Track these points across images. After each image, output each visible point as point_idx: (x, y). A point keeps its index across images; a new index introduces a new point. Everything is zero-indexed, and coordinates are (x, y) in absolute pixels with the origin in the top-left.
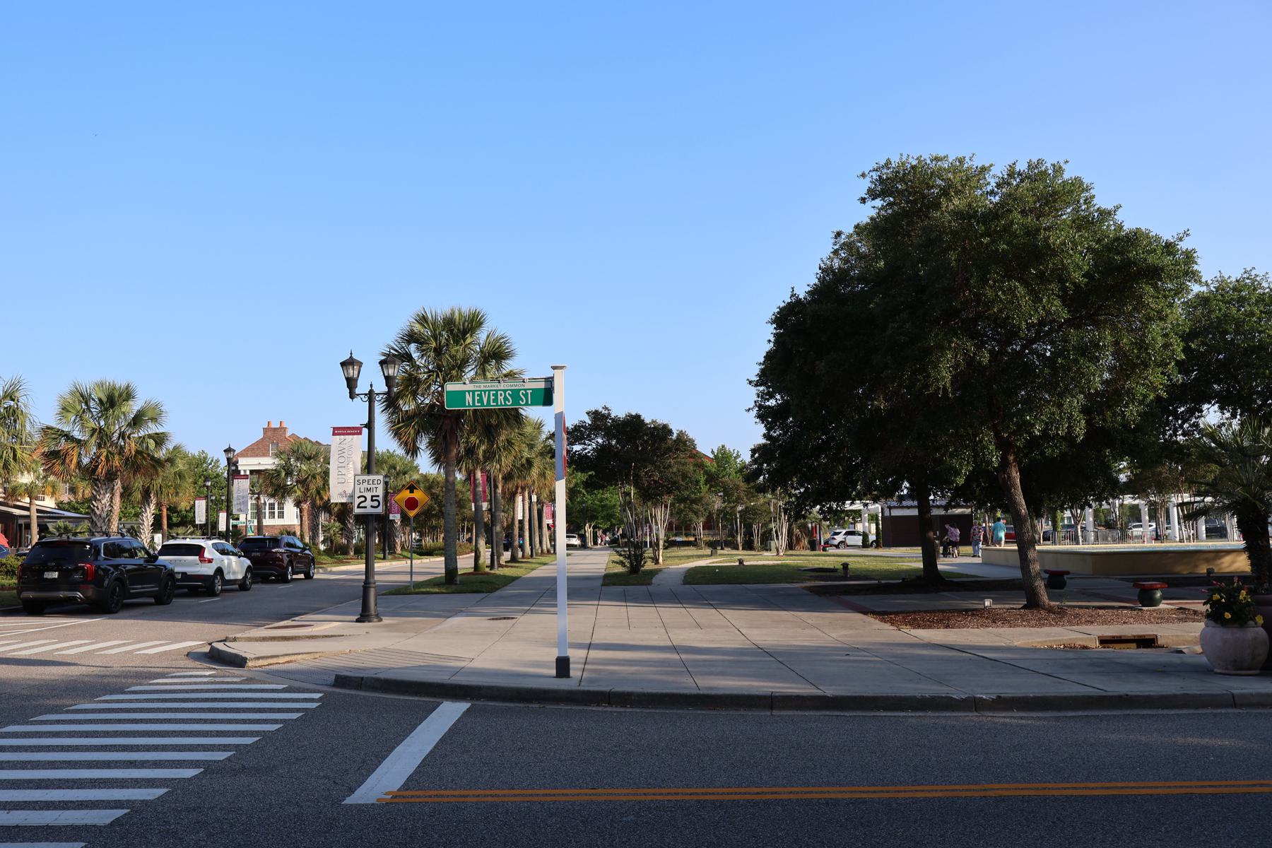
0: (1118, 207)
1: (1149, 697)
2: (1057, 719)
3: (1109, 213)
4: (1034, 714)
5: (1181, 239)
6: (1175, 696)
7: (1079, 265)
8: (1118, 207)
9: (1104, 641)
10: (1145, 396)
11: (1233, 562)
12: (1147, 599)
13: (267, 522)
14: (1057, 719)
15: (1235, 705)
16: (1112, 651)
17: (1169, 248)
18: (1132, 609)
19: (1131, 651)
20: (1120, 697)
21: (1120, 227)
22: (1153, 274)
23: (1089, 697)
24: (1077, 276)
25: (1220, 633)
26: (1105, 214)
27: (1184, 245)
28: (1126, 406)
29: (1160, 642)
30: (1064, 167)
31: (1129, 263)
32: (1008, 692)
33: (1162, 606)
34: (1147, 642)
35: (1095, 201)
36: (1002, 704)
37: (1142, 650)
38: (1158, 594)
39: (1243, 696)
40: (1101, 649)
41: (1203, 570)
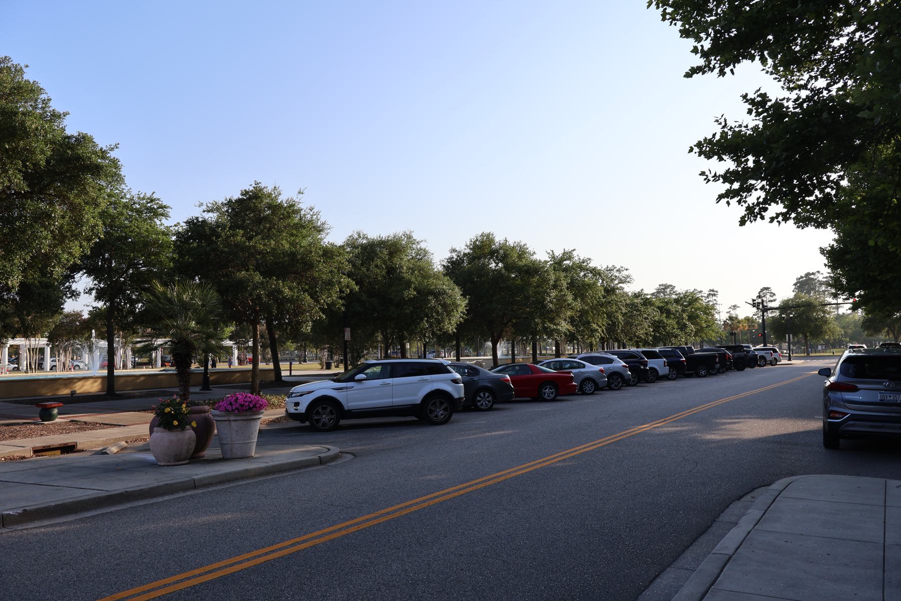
0: (65, 114)
1: (141, 490)
2: (82, 520)
3: (59, 117)
4: (46, 523)
5: (112, 149)
6: (158, 487)
7: (42, 154)
8: (65, 114)
9: (37, 451)
10: (68, 261)
11: (83, 386)
12: (46, 415)
13: (117, 372)
14: (82, 520)
15: (195, 487)
16: (47, 457)
17: (103, 154)
18: (35, 424)
19: (58, 455)
20: (122, 494)
21: (63, 130)
22: (96, 170)
23: (99, 498)
24: (41, 160)
25: (161, 435)
26: (56, 116)
27: (112, 155)
28: (54, 267)
29: (79, 447)
30: (25, 70)
31: (79, 158)
32: (31, 505)
33: (57, 420)
34: (68, 449)
35: (51, 104)
36: (28, 516)
37: (66, 456)
38: (55, 411)
39: (200, 480)
40: (35, 458)
41: (65, 392)
